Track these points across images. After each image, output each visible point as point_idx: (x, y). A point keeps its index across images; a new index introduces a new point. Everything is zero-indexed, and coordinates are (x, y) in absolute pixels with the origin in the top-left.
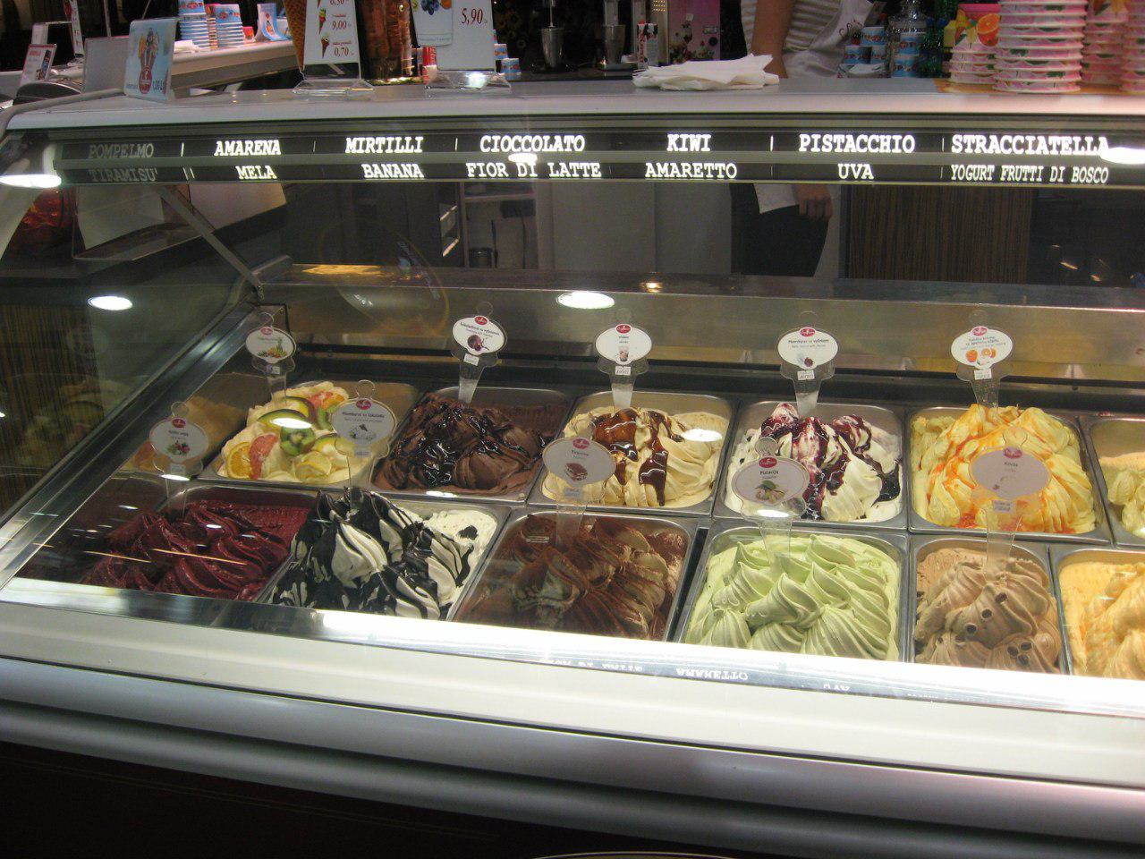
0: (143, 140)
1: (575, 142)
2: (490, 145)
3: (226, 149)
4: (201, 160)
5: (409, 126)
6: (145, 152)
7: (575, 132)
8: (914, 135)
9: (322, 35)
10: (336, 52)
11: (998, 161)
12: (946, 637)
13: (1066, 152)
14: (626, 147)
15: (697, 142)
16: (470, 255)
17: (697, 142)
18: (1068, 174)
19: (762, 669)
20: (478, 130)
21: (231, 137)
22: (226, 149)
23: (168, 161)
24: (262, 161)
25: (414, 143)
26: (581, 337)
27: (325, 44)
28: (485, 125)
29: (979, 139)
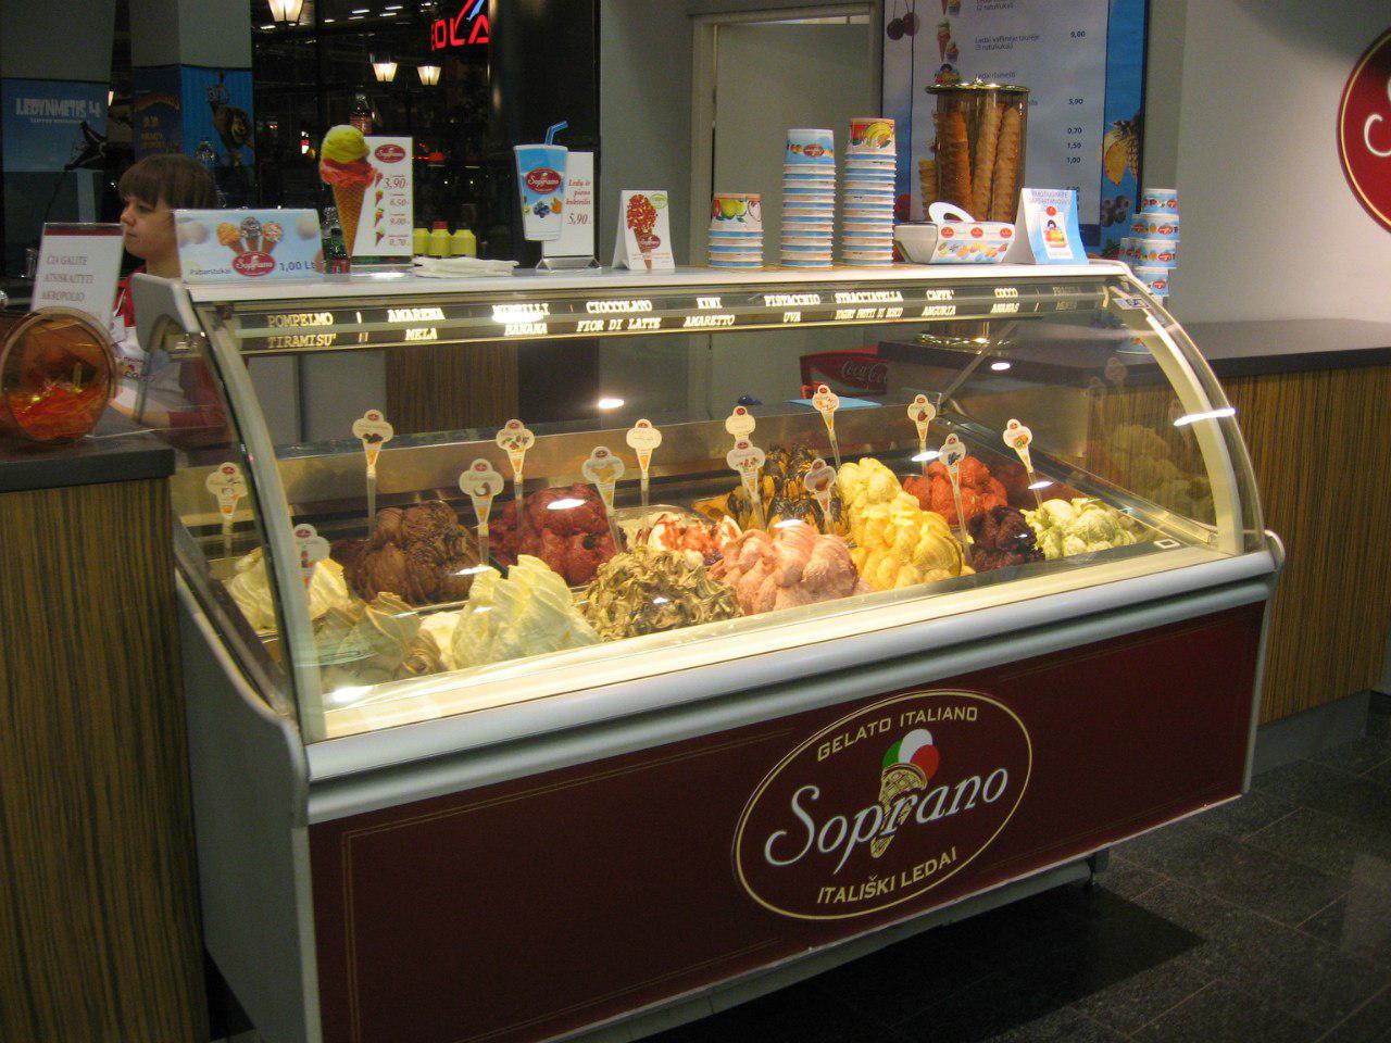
0: (321, 310)
1: (644, 305)
2: (593, 308)
3: (396, 317)
4: (376, 326)
5: (541, 296)
6: (324, 319)
7: (643, 298)
8: (331, 312)
9: (378, 229)
10: (392, 243)
11: (857, 307)
12: (1124, 445)
13: (885, 300)
14: (971, 294)
15: (713, 302)
16: (1167, 318)
17: (713, 302)
18: (625, 326)
19: (490, 671)
20: (585, 298)
21: (400, 306)
22: (396, 317)
23: (346, 328)
24: (428, 325)
25: (541, 308)
26: (553, 439)
27: (380, 236)
28: (496, 298)
29: (626, 303)
